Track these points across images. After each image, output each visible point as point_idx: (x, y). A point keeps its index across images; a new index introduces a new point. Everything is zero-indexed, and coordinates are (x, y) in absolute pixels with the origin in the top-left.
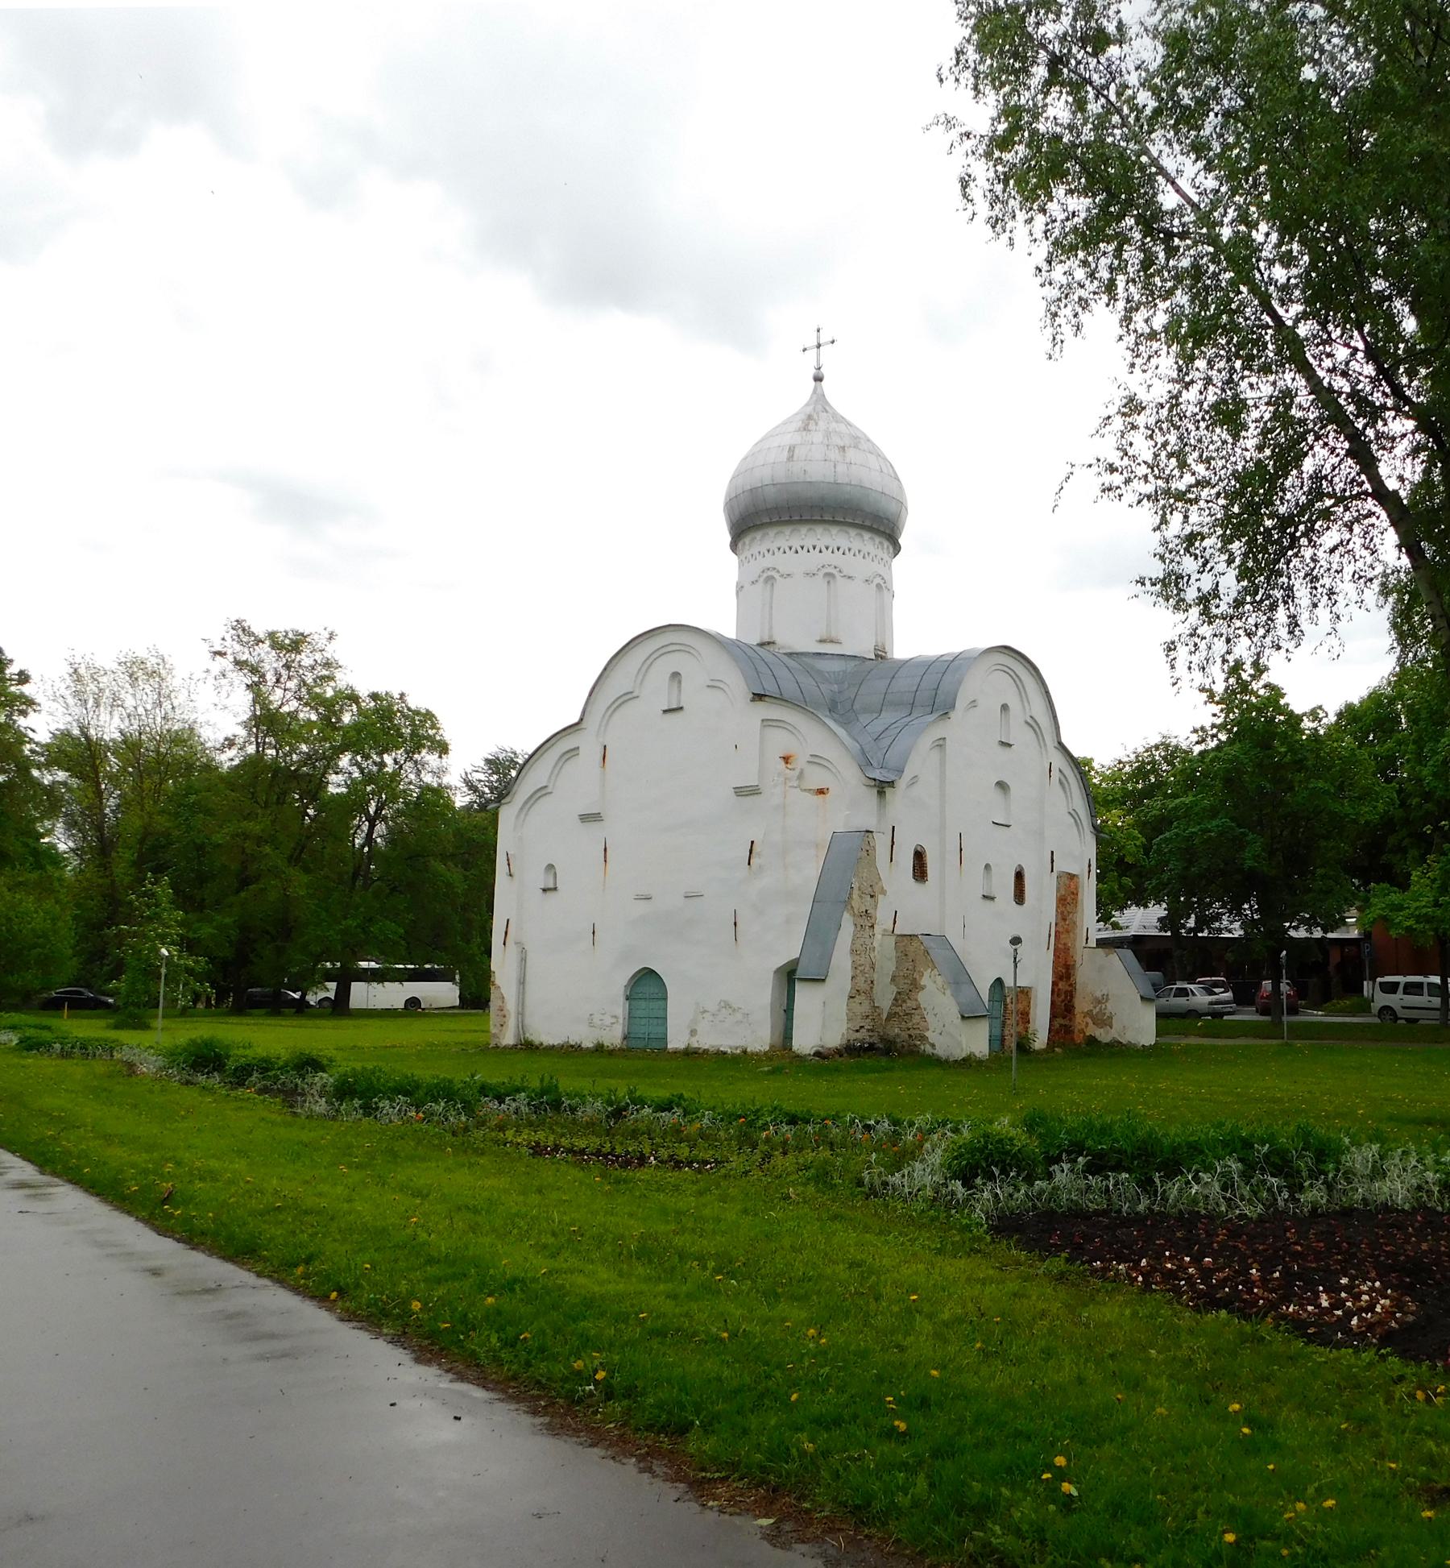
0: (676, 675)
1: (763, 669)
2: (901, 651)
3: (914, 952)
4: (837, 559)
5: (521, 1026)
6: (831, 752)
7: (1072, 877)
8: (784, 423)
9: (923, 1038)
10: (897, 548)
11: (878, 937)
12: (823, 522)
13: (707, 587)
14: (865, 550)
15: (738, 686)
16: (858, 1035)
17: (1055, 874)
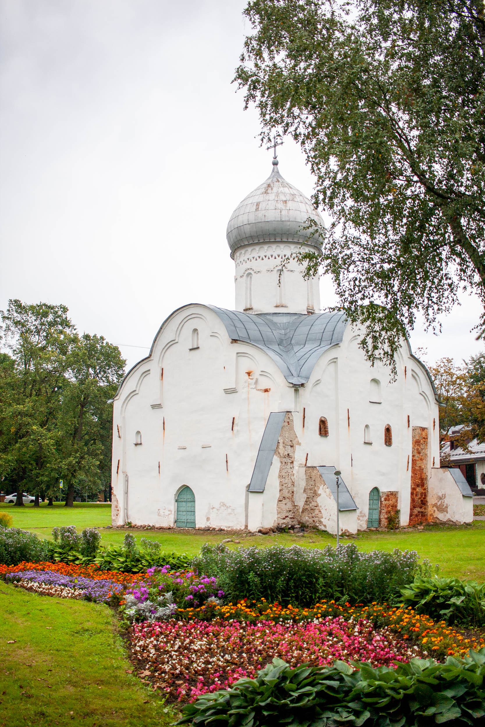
0: (195, 330)
5: (127, 516)
6: (271, 369)
7: (423, 429)
8: (256, 190)
9: (320, 522)
11: (296, 468)
12: (275, 242)
15: (224, 336)
16: (284, 521)
17: (411, 428)
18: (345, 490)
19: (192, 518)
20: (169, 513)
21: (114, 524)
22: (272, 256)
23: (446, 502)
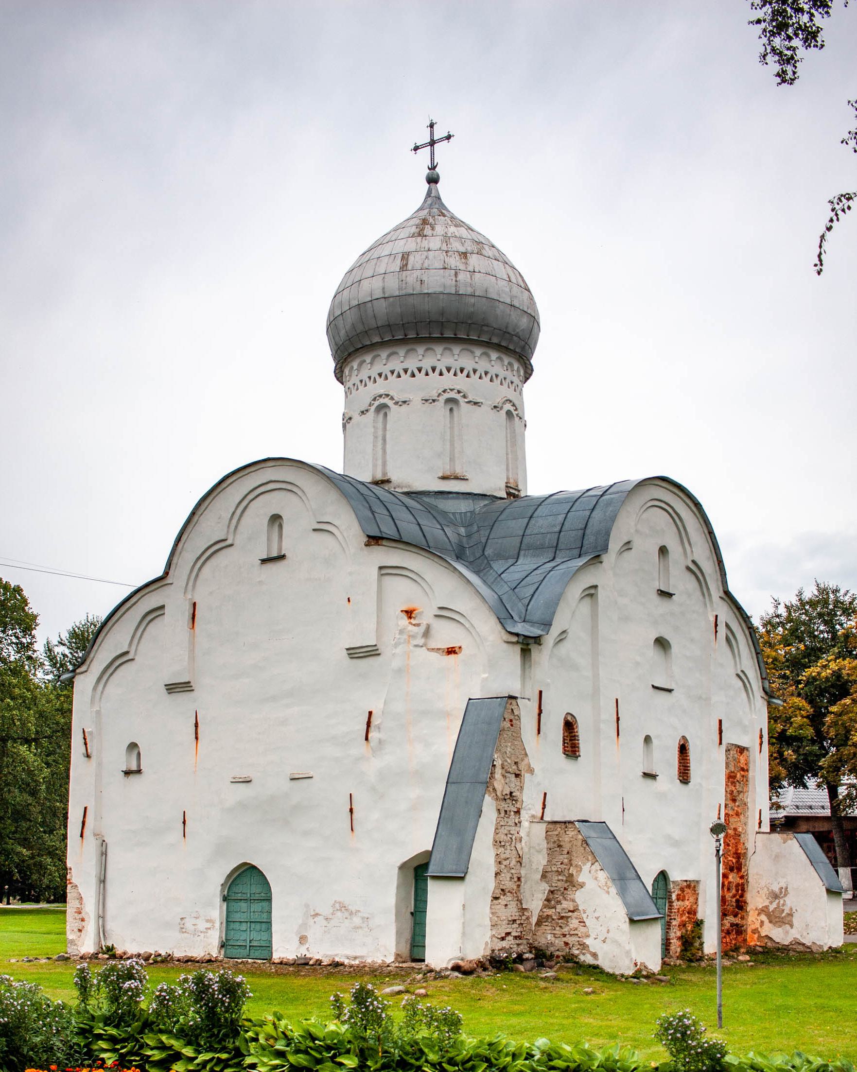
0: (276, 519)
1: (380, 510)
2: (537, 486)
3: (573, 841)
4: (461, 383)
5: (102, 931)
7: (742, 750)
8: (395, 229)
9: (584, 946)
10: (528, 372)
11: (525, 824)
12: (442, 340)
13: (308, 415)
14: (493, 371)
15: (348, 526)
16: (504, 944)
17: (724, 747)
18: (634, 875)
19: (264, 936)
20: (209, 925)
21: (72, 950)
22: (434, 369)
23: (788, 902)
